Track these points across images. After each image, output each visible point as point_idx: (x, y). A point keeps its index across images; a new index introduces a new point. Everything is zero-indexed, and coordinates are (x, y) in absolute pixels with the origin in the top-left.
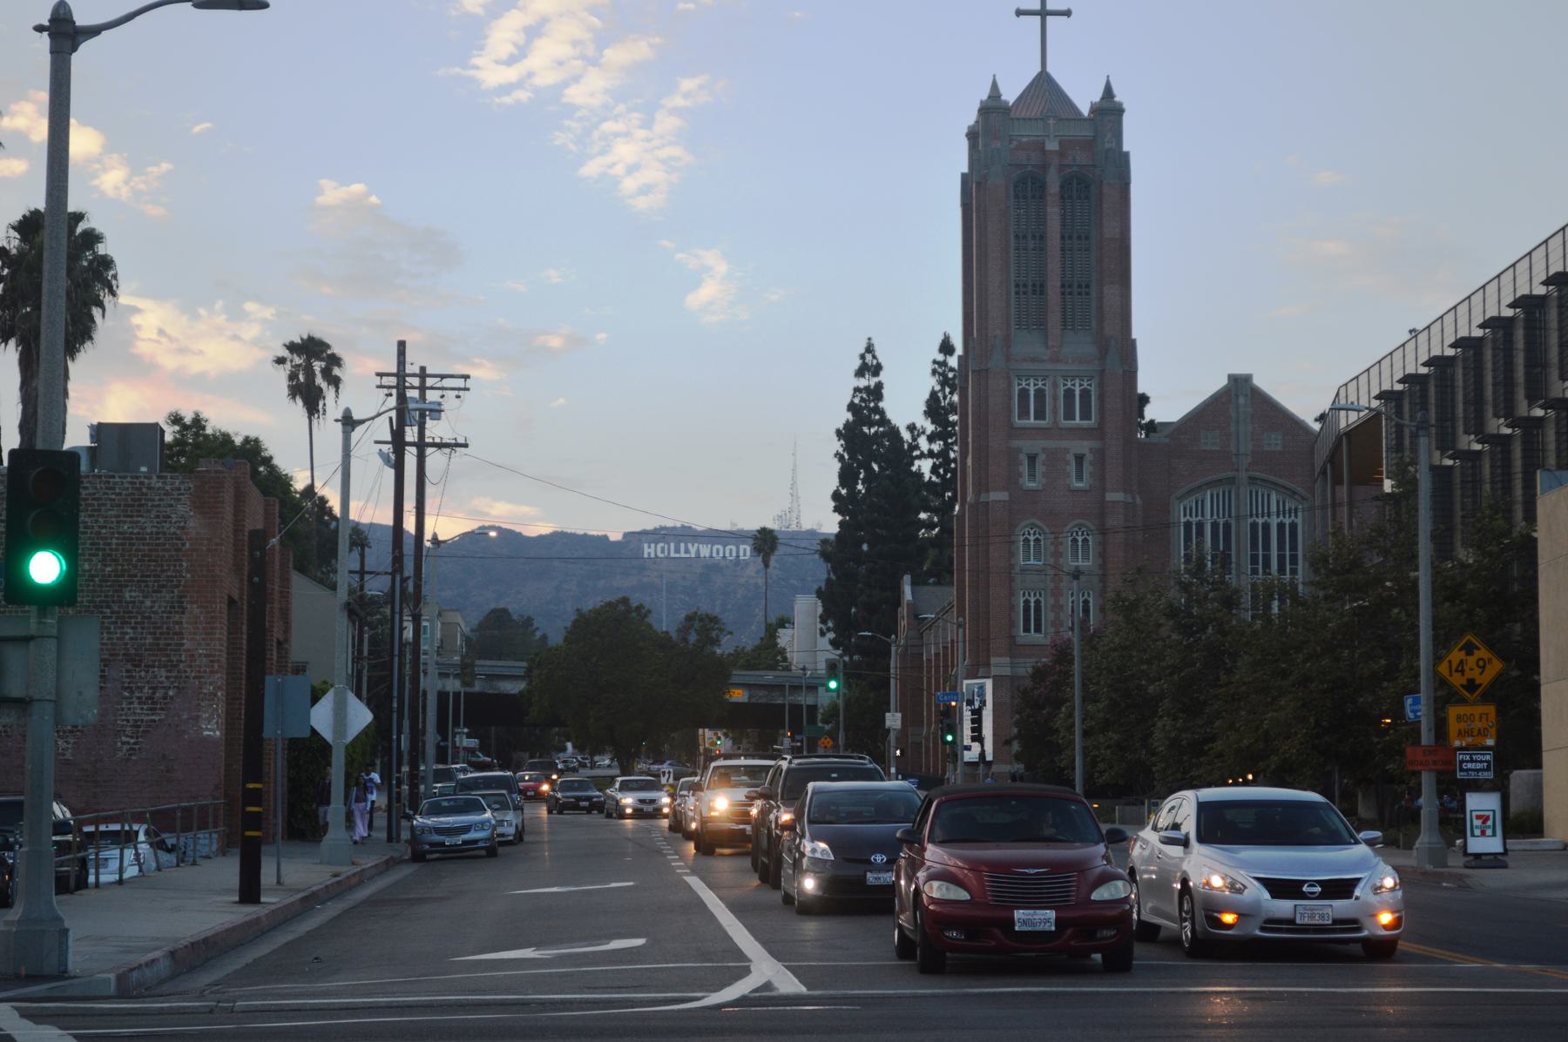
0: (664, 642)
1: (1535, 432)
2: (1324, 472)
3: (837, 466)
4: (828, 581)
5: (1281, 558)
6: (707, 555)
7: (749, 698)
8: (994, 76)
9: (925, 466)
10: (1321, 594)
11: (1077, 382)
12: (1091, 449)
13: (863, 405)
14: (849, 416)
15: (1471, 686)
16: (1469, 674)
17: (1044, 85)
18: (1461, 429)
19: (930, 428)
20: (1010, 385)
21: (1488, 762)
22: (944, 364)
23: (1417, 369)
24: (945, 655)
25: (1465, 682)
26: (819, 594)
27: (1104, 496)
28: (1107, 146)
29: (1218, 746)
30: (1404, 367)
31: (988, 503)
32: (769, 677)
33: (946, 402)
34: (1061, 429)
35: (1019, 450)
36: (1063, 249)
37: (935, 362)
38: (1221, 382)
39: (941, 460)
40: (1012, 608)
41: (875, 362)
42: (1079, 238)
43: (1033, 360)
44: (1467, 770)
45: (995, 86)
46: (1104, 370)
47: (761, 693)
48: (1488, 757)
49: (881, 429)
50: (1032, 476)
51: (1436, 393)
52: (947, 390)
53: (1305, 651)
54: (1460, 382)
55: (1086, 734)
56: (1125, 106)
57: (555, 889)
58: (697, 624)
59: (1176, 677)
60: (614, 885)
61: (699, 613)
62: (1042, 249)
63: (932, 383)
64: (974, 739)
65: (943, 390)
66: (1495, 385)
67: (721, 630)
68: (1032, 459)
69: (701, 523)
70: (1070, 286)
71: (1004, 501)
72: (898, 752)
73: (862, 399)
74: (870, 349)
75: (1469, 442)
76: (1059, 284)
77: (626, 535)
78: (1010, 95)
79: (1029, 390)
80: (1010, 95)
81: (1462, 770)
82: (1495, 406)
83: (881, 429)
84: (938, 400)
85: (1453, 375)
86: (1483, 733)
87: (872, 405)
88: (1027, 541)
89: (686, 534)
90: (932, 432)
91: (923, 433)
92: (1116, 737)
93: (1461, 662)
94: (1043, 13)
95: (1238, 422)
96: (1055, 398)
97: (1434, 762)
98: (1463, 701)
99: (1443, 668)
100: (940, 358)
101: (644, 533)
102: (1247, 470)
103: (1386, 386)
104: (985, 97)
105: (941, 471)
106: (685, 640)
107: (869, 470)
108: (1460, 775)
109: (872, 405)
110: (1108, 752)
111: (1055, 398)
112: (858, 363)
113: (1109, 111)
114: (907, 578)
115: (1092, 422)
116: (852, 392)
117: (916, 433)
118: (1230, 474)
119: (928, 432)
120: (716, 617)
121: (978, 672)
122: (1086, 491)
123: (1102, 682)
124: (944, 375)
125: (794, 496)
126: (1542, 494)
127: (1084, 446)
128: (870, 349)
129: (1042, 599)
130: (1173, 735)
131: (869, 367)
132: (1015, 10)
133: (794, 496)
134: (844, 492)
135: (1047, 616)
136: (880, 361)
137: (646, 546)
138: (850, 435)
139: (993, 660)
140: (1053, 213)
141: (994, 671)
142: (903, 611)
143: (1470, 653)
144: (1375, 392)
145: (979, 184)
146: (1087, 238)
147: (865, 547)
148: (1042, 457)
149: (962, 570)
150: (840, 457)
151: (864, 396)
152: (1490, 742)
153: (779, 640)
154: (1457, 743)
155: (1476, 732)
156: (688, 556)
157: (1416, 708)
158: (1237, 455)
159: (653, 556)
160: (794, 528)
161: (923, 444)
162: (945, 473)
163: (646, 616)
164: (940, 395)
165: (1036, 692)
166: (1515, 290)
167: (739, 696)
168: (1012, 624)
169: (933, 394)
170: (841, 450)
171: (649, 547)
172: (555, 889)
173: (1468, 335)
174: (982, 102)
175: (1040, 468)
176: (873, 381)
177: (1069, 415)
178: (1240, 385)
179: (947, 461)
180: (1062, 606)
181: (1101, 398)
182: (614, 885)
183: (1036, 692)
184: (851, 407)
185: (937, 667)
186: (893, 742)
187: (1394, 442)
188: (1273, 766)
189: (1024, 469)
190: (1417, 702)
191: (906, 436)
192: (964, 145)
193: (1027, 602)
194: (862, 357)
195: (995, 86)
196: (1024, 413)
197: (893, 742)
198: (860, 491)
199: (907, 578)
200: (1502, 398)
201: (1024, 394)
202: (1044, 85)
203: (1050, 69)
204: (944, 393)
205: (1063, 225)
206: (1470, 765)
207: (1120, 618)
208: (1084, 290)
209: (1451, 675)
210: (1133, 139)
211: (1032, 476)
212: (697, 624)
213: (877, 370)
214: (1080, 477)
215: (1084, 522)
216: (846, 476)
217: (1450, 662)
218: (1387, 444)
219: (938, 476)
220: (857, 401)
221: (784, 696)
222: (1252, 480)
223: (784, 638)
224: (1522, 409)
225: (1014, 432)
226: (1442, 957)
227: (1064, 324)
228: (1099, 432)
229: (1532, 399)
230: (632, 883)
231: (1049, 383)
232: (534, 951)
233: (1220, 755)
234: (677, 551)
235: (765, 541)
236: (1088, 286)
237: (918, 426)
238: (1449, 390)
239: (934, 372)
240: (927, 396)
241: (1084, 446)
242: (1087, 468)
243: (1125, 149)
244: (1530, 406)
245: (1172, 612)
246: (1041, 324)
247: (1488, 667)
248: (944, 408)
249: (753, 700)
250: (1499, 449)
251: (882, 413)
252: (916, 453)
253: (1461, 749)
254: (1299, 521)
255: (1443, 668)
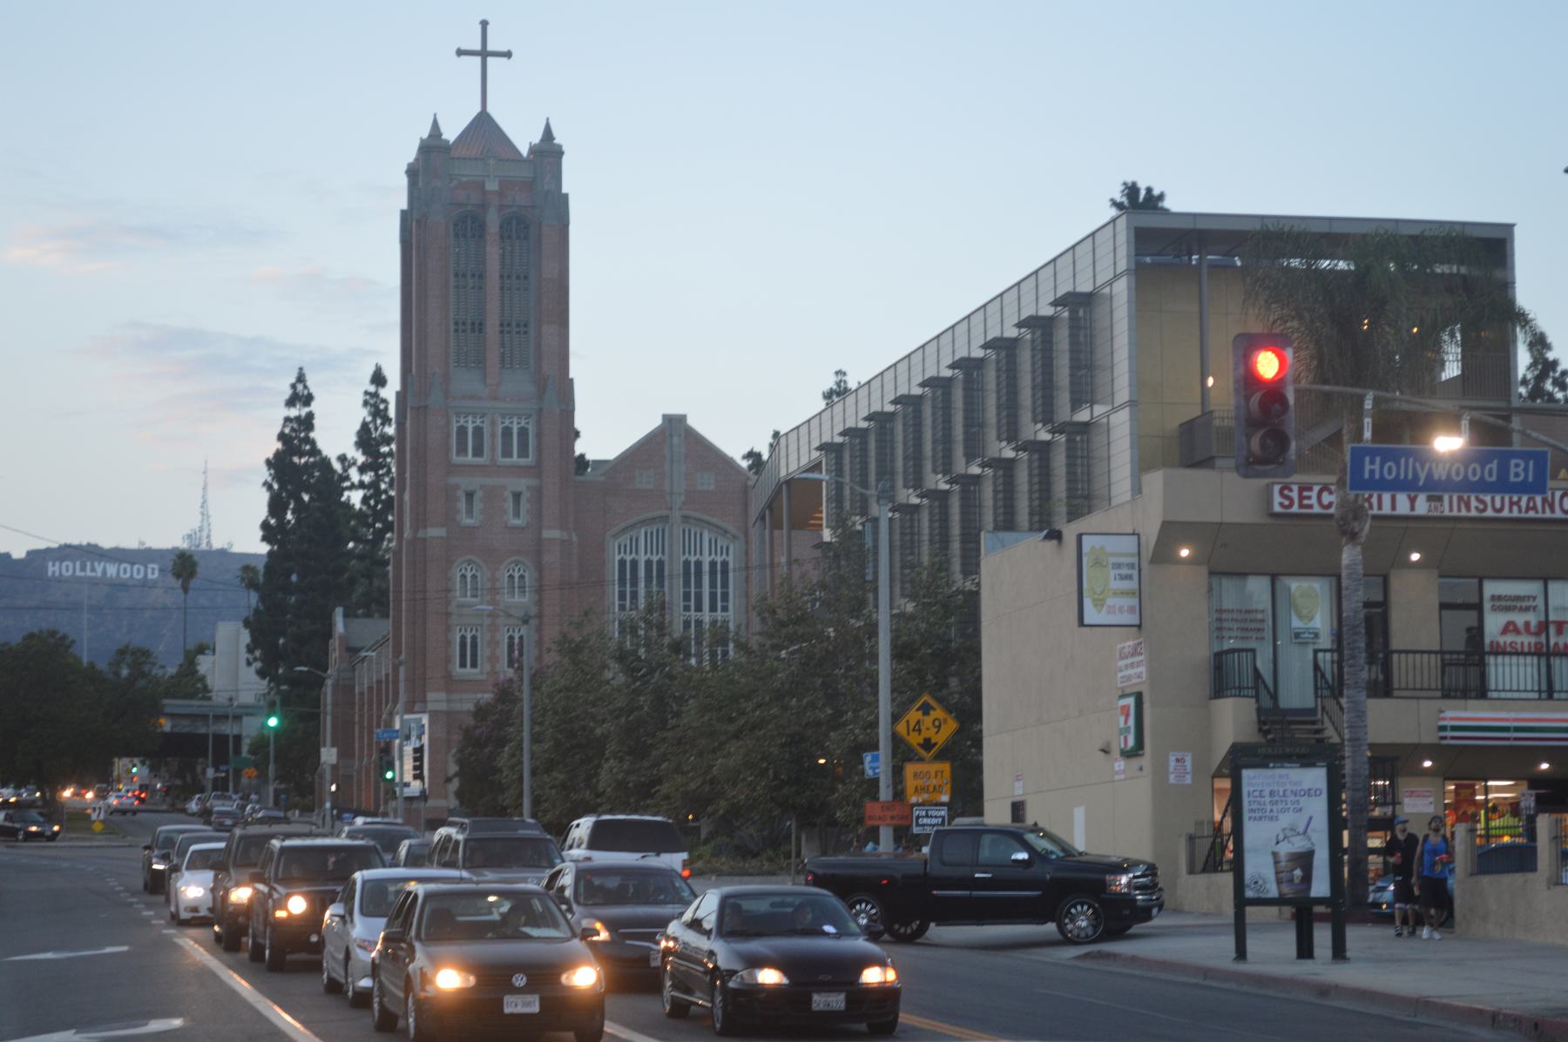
0: (92, 674)
1: (972, 488)
2: (762, 518)
3: (265, 496)
4: (257, 611)
5: (713, 596)
6: (114, 575)
7: (172, 727)
8: (435, 115)
9: (355, 498)
10: (769, 643)
11: (515, 420)
12: (528, 487)
13: (294, 435)
14: (279, 445)
15: (927, 745)
16: (925, 734)
17: (483, 126)
18: (900, 483)
19: (361, 458)
20: (448, 423)
21: (943, 818)
22: (375, 395)
23: (857, 423)
24: (379, 690)
25: (922, 742)
26: (247, 623)
27: (540, 532)
28: (546, 188)
29: (665, 788)
30: (844, 420)
31: (425, 539)
32: (194, 705)
33: (378, 433)
34: (499, 466)
35: (457, 487)
36: (502, 289)
37: (366, 393)
38: (657, 422)
39: (371, 491)
40: (448, 643)
41: (306, 392)
42: (518, 278)
43: (472, 397)
44: (923, 825)
45: (435, 125)
46: (541, 410)
47: (185, 722)
48: (943, 813)
49: (312, 460)
50: (470, 512)
51: (876, 447)
52: (379, 421)
53: (755, 701)
54: (899, 437)
55: (534, 773)
56: (564, 148)
57: (50, 955)
58: (129, 658)
59: (623, 720)
60: (109, 950)
61: (131, 647)
62: (480, 288)
63: (364, 414)
64: (415, 777)
65: (374, 420)
66: (934, 442)
67: (154, 664)
68: (470, 496)
69: (107, 543)
70: (509, 325)
71: (442, 538)
72: (333, 788)
73: (293, 429)
74: (301, 378)
75: (908, 496)
76: (498, 322)
77: (29, 553)
78: (451, 133)
79: (467, 428)
80: (451, 133)
81: (918, 825)
82: (934, 462)
83: (312, 460)
84: (369, 431)
85: (892, 429)
86: (937, 789)
87: (302, 435)
88: (464, 577)
89: (92, 553)
90: (363, 463)
91: (354, 463)
92: (561, 777)
93: (918, 722)
94: (484, 54)
95: (672, 461)
96: (493, 435)
97: (892, 818)
98: (921, 760)
99: (901, 728)
100: (372, 389)
101: (48, 551)
102: (680, 509)
103: (826, 438)
104: (425, 135)
105: (372, 502)
106: (117, 674)
107: (299, 500)
108: (916, 830)
109: (302, 435)
110: (554, 791)
111: (493, 435)
112: (288, 392)
113: (548, 153)
114: (339, 612)
115: (530, 460)
116: (282, 422)
117: (347, 464)
118: (664, 512)
119: (360, 462)
120: (148, 651)
121: (413, 707)
122: (523, 528)
123: (547, 723)
124: (375, 406)
125: (205, 515)
126: (986, 555)
127: (522, 484)
128: (301, 378)
129: (479, 635)
130: (620, 777)
131: (300, 397)
132: (455, 49)
133: (205, 515)
134: (272, 521)
135: (483, 652)
136: (311, 391)
137: (50, 564)
138: (279, 465)
139: (431, 696)
140: (493, 252)
141: (430, 706)
142: (335, 643)
143: (926, 713)
144: (816, 444)
145: (419, 222)
146: (526, 278)
147: (294, 578)
148: (479, 495)
149: (398, 601)
150: (269, 486)
151: (295, 426)
152: (945, 798)
153: (199, 668)
154: (914, 800)
155: (931, 789)
156: (93, 574)
157: (876, 765)
158: (671, 494)
159: (57, 574)
160: (204, 546)
161: (354, 475)
162: (376, 505)
163: (69, 647)
164: (371, 426)
165: (478, 732)
166: (953, 352)
167: (166, 725)
168: (448, 660)
169: (365, 426)
170: (269, 479)
171: (54, 565)
172: (50, 955)
173: (907, 393)
174: (422, 140)
175: (478, 505)
176: (304, 411)
177: (507, 453)
178: (674, 426)
179: (378, 492)
180: (498, 643)
181: (539, 435)
182: (109, 950)
183: (478, 732)
184: (282, 437)
185: (370, 701)
186: (328, 776)
187: (834, 492)
188: (721, 812)
189: (462, 505)
190: (875, 759)
191: (337, 466)
192: (403, 181)
193: (463, 638)
194: (293, 386)
195: (435, 125)
196: (462, 450)
197: (328, 776)
198: (289, 522)
199: (339, 612)
200: (940, 455)
201: (462, 431)
202: (483, 126)
203: (490, 109)
204: (376, 424)
205: (503, 265)
206: (925, 821)
207: (566, 660)
208: (522, 329)
209: (908, 734)
210: (572, 181)
211: (470, 512)
212: (129, 658)
213: (308, 400)
214: (517, 514)
215: (521, 559)
216: (276, 506)
217: (908, 722)
218: (827, 495)
219: (369, 505)
220: (287, 431)
221: (208, 726)
222: (686, 518)
223: (204, 664)
224: (960, 466)
225: (452, 469)
226: (950, 1033)
227: (503, 362)
228: (537, 470)
229: (970, 457)
230: (125, 948)
231: (487, 420)
232: (76, 1033)
233: (667, 797)
234: (83, 569)
235: (184, 565)
236: (526, 326)
237: (349, 456)
238: (977, 510)
239: (366, 403)
240: (357, 427)
241: (522, 484)
242: (524, 505)
243: (564, 190)
244: (968, 462)
245: (622, 656)
246: (481, 363)
247: (943, 726)
248: (375, 439)
249: (176, 730)
250: (937, 503)
251: (313, 443)
252: (347, 484)
253: (919, 805)
254: (731, 559)
255: (901, 728)
